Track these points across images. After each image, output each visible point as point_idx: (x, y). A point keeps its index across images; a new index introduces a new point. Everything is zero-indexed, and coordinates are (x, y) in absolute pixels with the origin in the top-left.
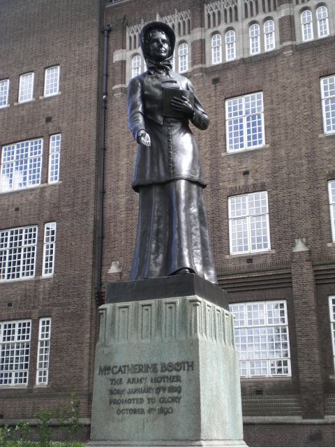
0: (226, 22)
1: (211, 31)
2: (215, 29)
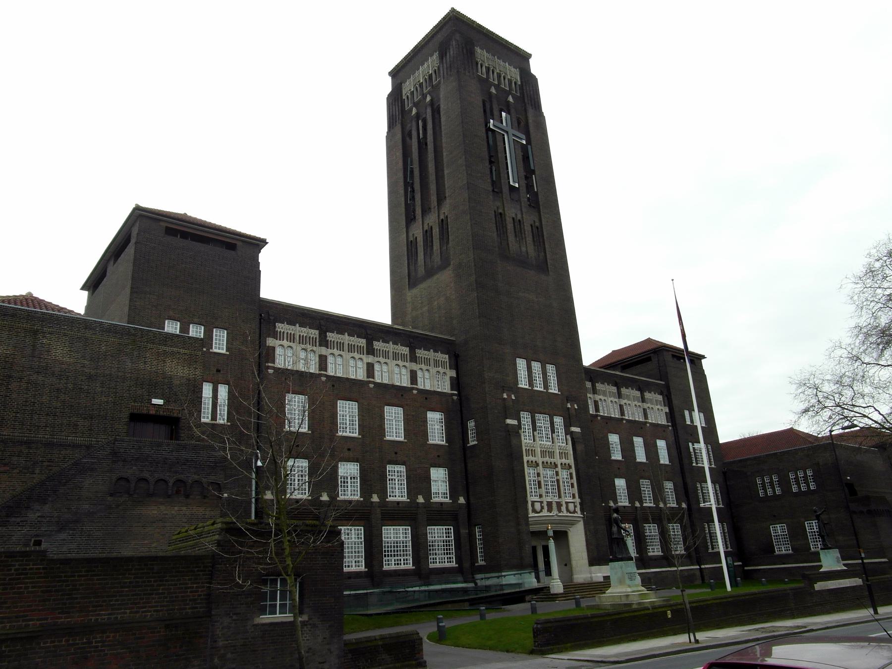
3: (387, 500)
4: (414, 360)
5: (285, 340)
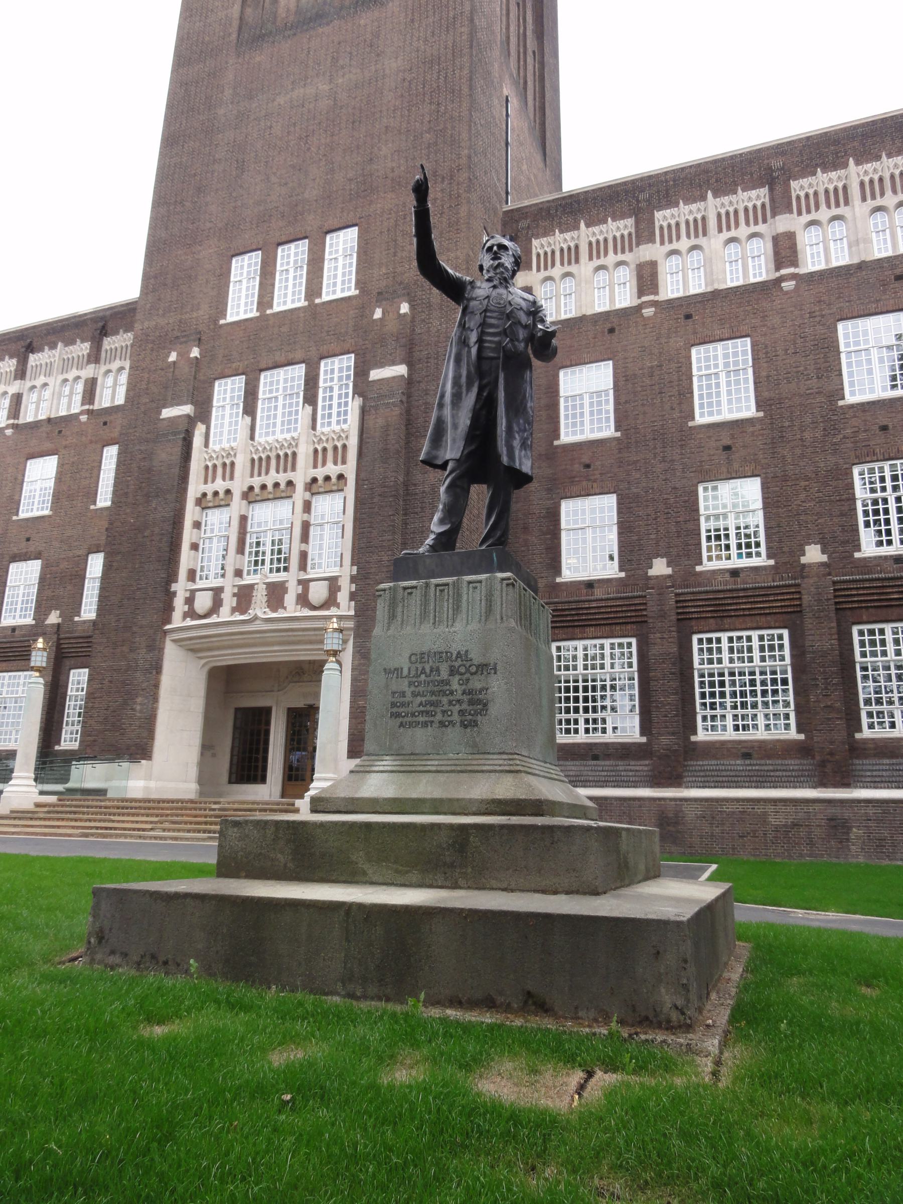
0: (829, 207)
1: (668, 247)
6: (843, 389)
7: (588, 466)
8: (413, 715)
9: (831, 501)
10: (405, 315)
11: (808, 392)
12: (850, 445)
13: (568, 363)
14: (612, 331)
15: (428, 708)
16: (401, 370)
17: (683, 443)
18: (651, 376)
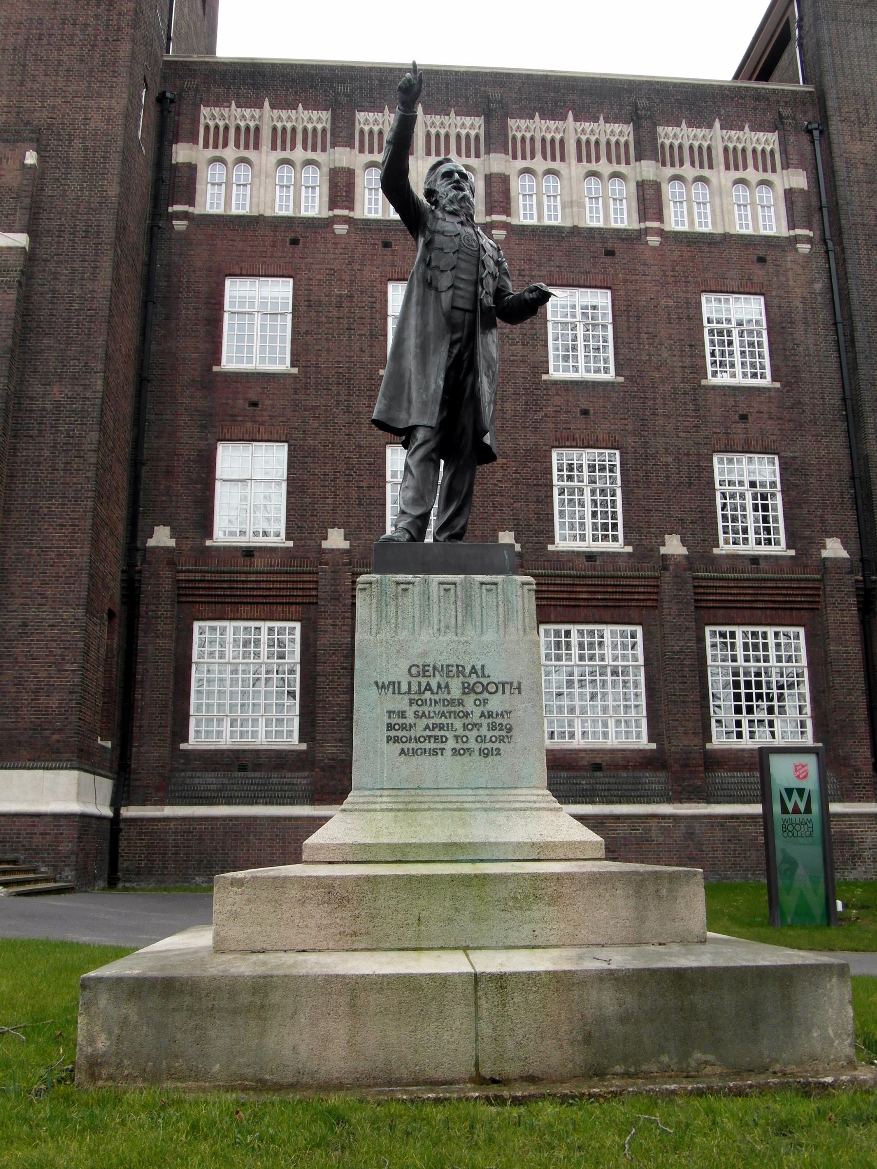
1: (211, 153)
2: (217, 153)
3: (716, 551)
4: (648, 153)
5: (603, 159)
6: (547, 362)
7: (255, 404)
8: (417, 740)
9: (528, 485)
10: (32, 167)
11: (512, 358)
12: (551, 425)
13: (238, 272)
14: (295, 242)
15: (437, 732)
16: (21, 240)
17: (373, 393)
18: (339, 306)
